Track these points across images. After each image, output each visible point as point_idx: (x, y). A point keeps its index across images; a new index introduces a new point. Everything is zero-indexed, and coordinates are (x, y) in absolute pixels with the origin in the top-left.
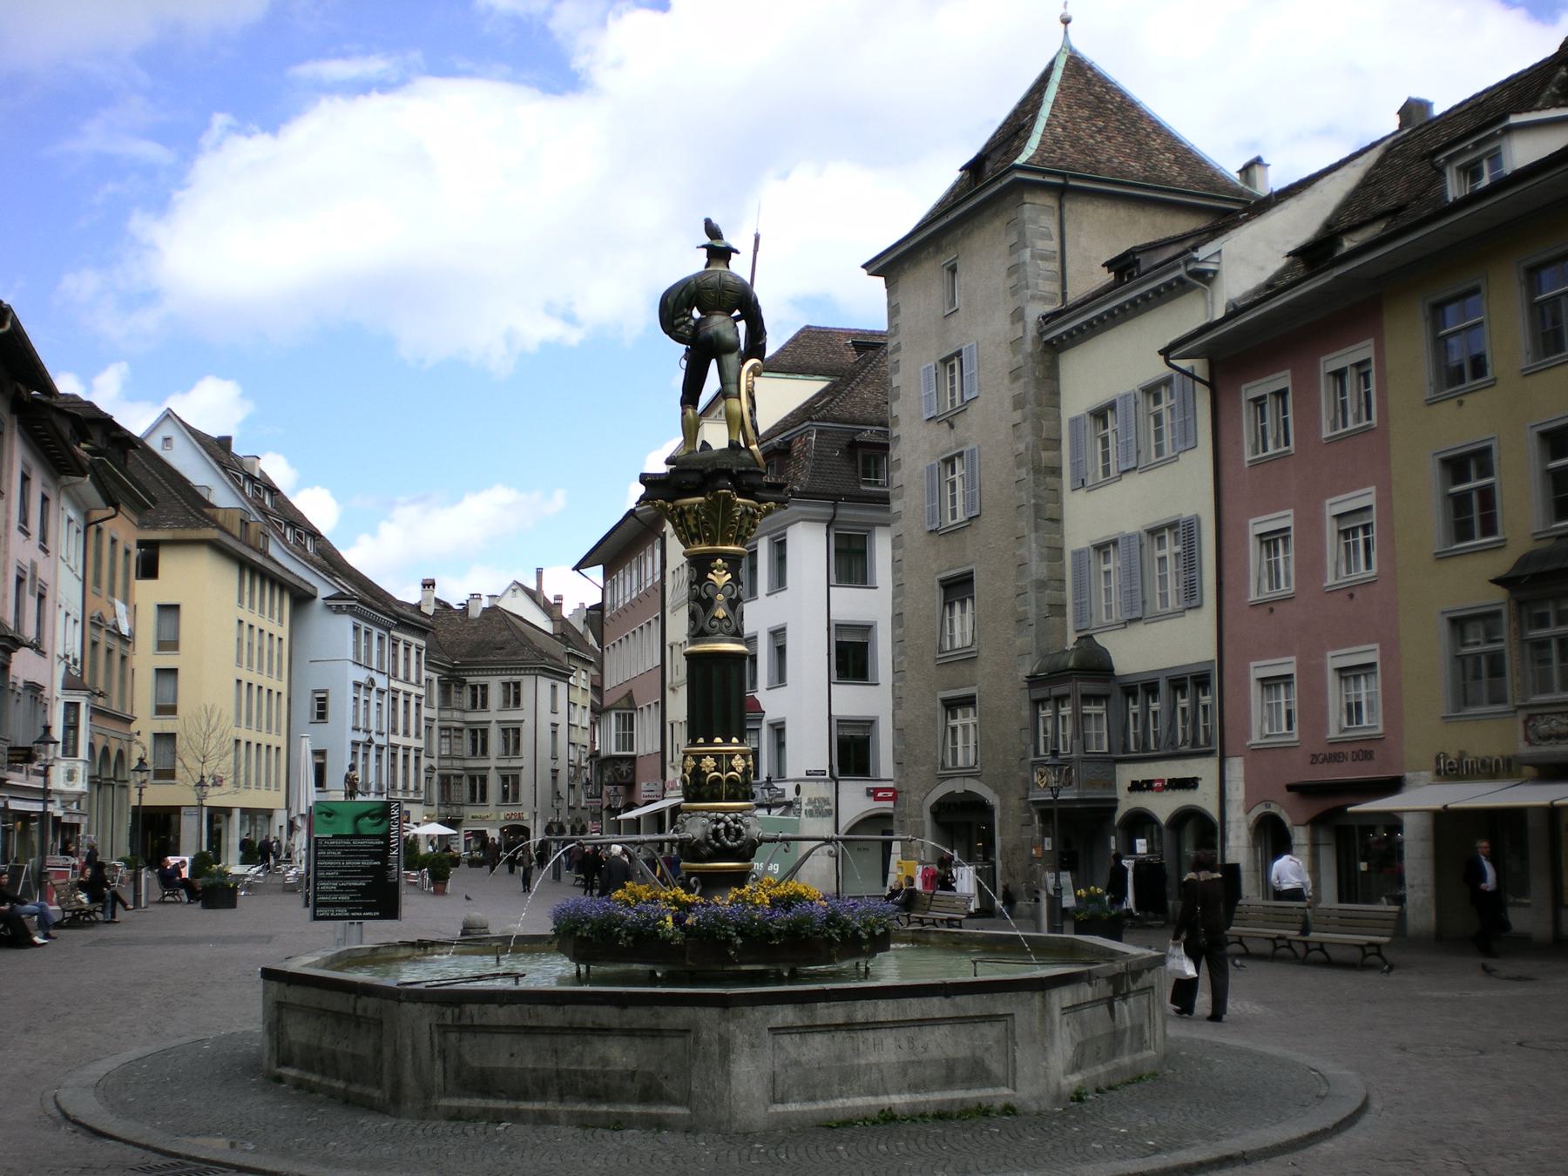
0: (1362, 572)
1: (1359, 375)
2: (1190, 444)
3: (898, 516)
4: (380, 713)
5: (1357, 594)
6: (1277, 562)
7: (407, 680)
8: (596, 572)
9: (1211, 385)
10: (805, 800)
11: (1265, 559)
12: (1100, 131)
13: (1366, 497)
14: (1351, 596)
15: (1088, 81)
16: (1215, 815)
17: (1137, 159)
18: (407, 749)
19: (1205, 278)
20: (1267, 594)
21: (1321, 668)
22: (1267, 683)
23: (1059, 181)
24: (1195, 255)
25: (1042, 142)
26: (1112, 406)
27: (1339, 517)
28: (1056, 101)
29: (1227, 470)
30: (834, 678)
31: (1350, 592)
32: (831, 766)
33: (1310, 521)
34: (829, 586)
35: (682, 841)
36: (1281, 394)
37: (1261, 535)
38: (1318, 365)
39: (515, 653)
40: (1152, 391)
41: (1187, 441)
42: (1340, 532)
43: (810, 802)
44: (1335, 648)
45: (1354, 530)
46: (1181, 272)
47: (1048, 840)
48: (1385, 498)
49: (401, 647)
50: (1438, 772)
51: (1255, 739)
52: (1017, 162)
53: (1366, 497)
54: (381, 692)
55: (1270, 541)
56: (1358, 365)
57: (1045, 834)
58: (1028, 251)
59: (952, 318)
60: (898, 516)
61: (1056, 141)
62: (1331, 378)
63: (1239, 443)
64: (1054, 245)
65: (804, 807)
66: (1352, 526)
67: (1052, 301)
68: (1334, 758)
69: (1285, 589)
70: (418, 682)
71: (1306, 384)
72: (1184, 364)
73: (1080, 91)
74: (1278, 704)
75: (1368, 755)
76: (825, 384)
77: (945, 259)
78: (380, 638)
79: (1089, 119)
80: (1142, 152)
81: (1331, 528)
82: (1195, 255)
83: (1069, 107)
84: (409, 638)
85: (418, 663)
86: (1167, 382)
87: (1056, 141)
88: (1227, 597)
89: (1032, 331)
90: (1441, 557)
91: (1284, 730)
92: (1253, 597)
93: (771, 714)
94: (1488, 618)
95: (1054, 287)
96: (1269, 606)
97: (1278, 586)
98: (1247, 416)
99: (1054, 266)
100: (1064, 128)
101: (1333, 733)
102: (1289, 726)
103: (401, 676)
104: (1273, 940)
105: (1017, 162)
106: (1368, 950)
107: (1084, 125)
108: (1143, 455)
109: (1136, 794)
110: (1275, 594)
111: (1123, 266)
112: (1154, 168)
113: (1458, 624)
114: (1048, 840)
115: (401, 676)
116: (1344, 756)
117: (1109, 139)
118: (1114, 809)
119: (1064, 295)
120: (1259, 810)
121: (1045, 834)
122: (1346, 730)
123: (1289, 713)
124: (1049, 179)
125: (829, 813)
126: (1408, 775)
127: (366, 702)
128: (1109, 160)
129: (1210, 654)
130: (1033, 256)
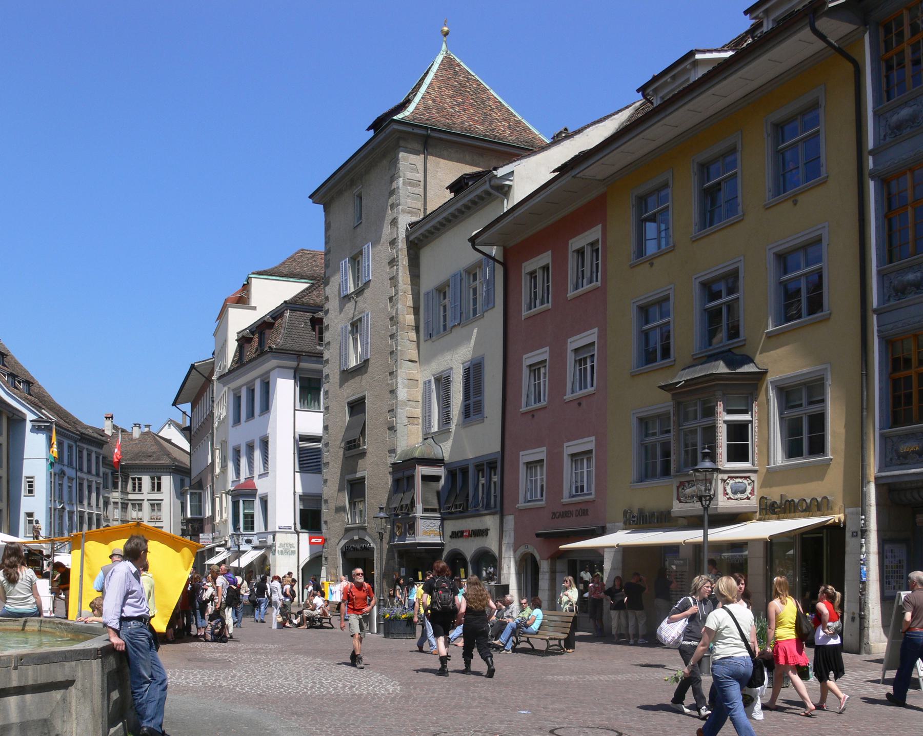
0: (590, 390)
1: (593, 251)
2: (491, 305)
3: (327, 361)
4: (70, 492)
5: (584, 403)
6: (539, 384)
7: (89, 472)
8: (187, 407)
9: (505, 265)
10: (278, 544)
11: (532, 383)
12: (459, 105)
13: (591, 336)
14: (580, 404)
15: (456, 73)
16: (497, 554)
17: (482, 124)
18: (81, 513)
19: (505, 191)
20: (533, 406)
21: (561, 453)
22: (529, 465)
23: (424, 132)
24: (495, 173)
25: (416, 108)
26: (447, 284)
27: (576, 350)
28: (431, 84)
29: (512, 322)
30: (297, 469)
31: (579, 402)
32: (295, 524)
33: (558, 355)
34: (295, 410)
35: (759, 642)
36: (545, 268)
37: (530, 366)
38: (567, 244)
39: (158, 460)
40: (471, 272)
41: (489, 302)
42: (575, 361)
43: (281, 545)
44: (569, 441)
45: (585, 359)
46: (487, 187)
47: (403, 569)
48: (602, 336)
49: (85, 453)
50: (625, 523)
51: (521, 504)
52: (395, 118)
53: (591, 336)
54: (70, 479)
55: (534, 369)
56: (592, 244)
57: (401, 565)
58: (401, 179)
59: (358, 229)
60: (327, 361)
61: (427, 108)
62: (575, 255)
63: (520, 304)
64: (420, 176)
65: (277, 549)
66: (583, 355)
67: (416, 214)
68: (566, 514)
69: (543, 403)
70: (98, 475)
71: (560, 259)
72: (485, 249)
73: (449, 79)
74: (536, 480)
75: (585, 513)
76: (307, 285)
77: (356, 191)
78: (70, 447)
79: (452, 97)
80: (486, 118)
81: (571, 358)
82: (495, 173)
83: (440, 88)
84: (90, 447)
85: (97, 463)
86: (479, 265)
87: (427, 108)
88: (509, 408)
89: (402, 234)
90: (633, 375)
91: (539, 497)
92: (524, 409)
93: (261, 491)
94: (663, 418)
95: (420, 205)
96: (532, 414)
97: (539, 401)
98: (525, 282)
99: (420, 190)
100: (434, 101)
101: (566, 499)
102: (542, 496)
103: (85, 469)
104: (547, 640)
105: (395, 118)
106: (551, 643)
107: (448, 100)
108: (464, 315)
109: (454, 540)
110: (538, 405)
111: (457, 187)
112: (493, 130)
113: (644, 423)
114: (403, 569)
115: (85, 469)
116: (571, 513)
117: (464, 110)
118: (442, 550)
119: (425, 210)
120: (522, 550)
121: (401, 565)
122: (574, 496)
123: (542, 486)
124: (416, 131)
125: (293, 552)
126: (608, 525)
127: (70, 487)
128: (462, 123)
129: (498, 449)
130: (404, 183)
